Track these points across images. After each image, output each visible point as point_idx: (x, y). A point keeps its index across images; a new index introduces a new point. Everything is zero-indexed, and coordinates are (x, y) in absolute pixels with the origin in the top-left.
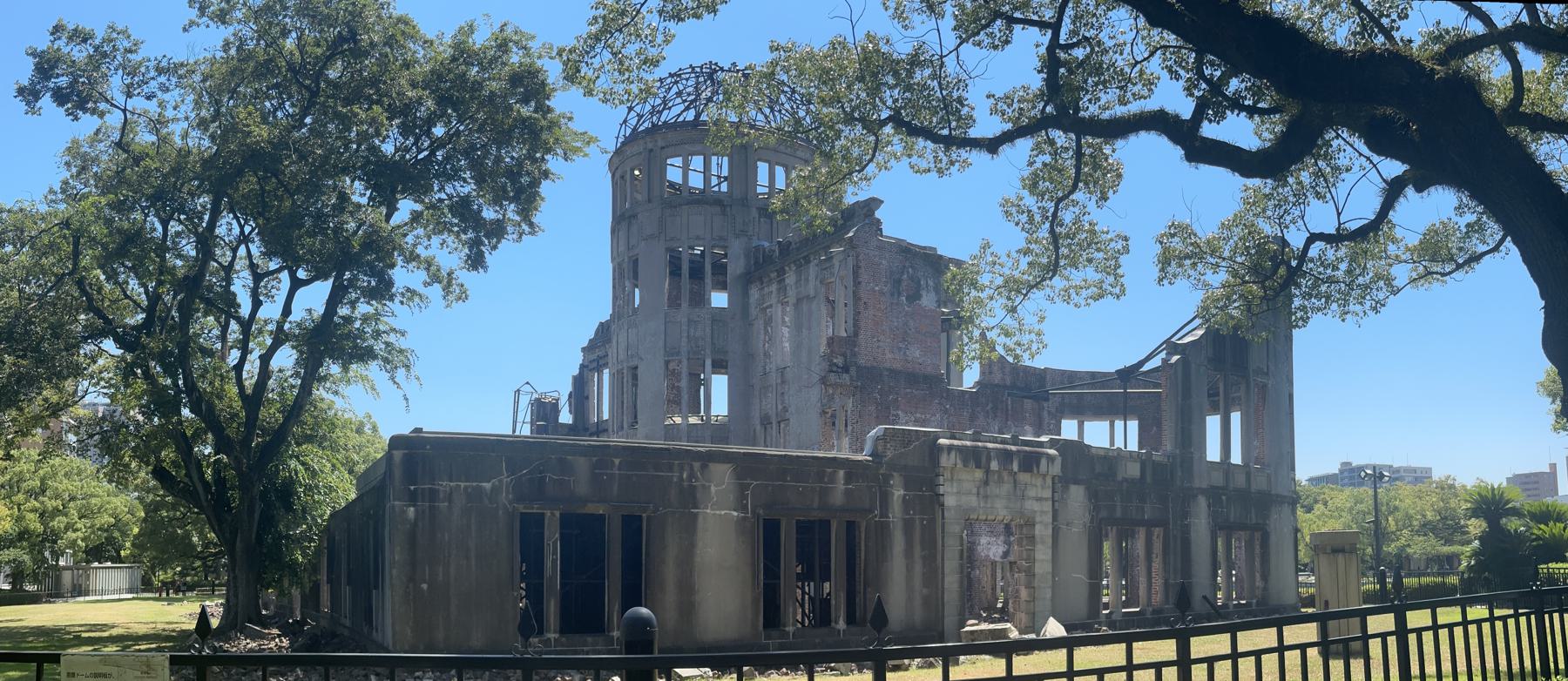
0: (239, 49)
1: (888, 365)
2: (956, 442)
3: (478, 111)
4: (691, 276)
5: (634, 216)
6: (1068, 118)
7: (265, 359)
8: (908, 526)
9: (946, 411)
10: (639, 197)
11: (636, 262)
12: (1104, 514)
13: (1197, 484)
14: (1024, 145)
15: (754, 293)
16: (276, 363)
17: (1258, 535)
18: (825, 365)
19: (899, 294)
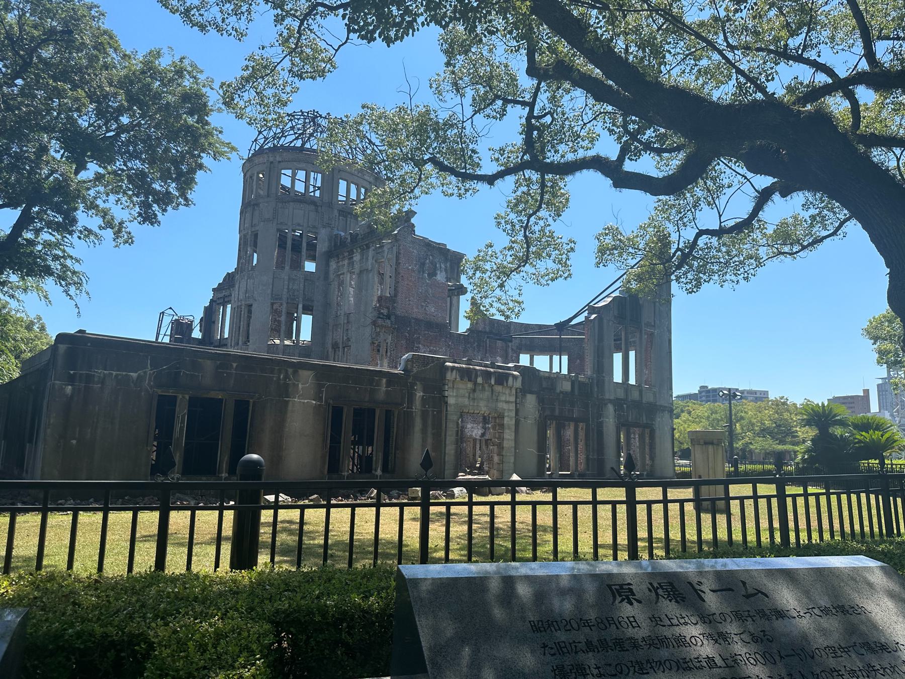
1: (414, 316)
2: (456, 365)
4: (292, 249)
5: (257, 205)
10: (261, 192)
11: (256, 236)
12: (548, 413)
13: (607, 396)
14: (510, 179)
15: (333, 265)
17: (647, 431)
18: (376, 314)
19: (424, 272)
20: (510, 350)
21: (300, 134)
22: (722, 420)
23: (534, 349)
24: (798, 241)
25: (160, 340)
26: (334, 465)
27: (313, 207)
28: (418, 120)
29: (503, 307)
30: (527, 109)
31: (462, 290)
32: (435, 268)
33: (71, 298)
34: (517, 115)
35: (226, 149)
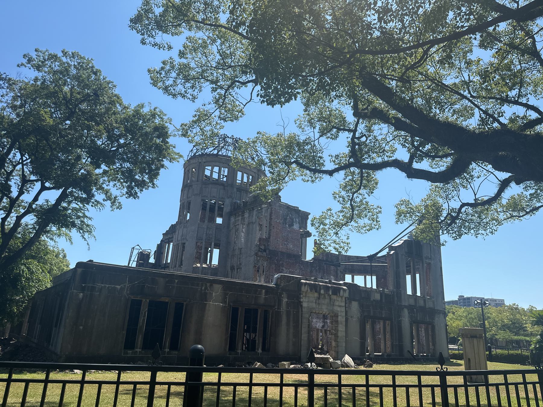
0: (43, 83)
1: (280, 250)
2: (308, 282)
3: (139, 137)
5: (191, 186)
6: (357, 163)
7: (19, 218)
9: (301, 269)
10: (193, 179)
13: (403, 304)
14: (342, 173)
15: (233, 219)
16: (23, 221)
17: (430, 326)
19: (286, 224)
20: (339, 272)
21: (216, 147)
22: (475, 318)
23: (354, 271)
24: (523, 209)
25: (130, 265)
26: (232, 346)
27: (222, 187)
28: (288, 141)
29: (337, 246)
30: (352, 134)
31: (309, 234)
32: (293, 222)
33: (85, 240)
34: (345, 137)
35: (177, 156)
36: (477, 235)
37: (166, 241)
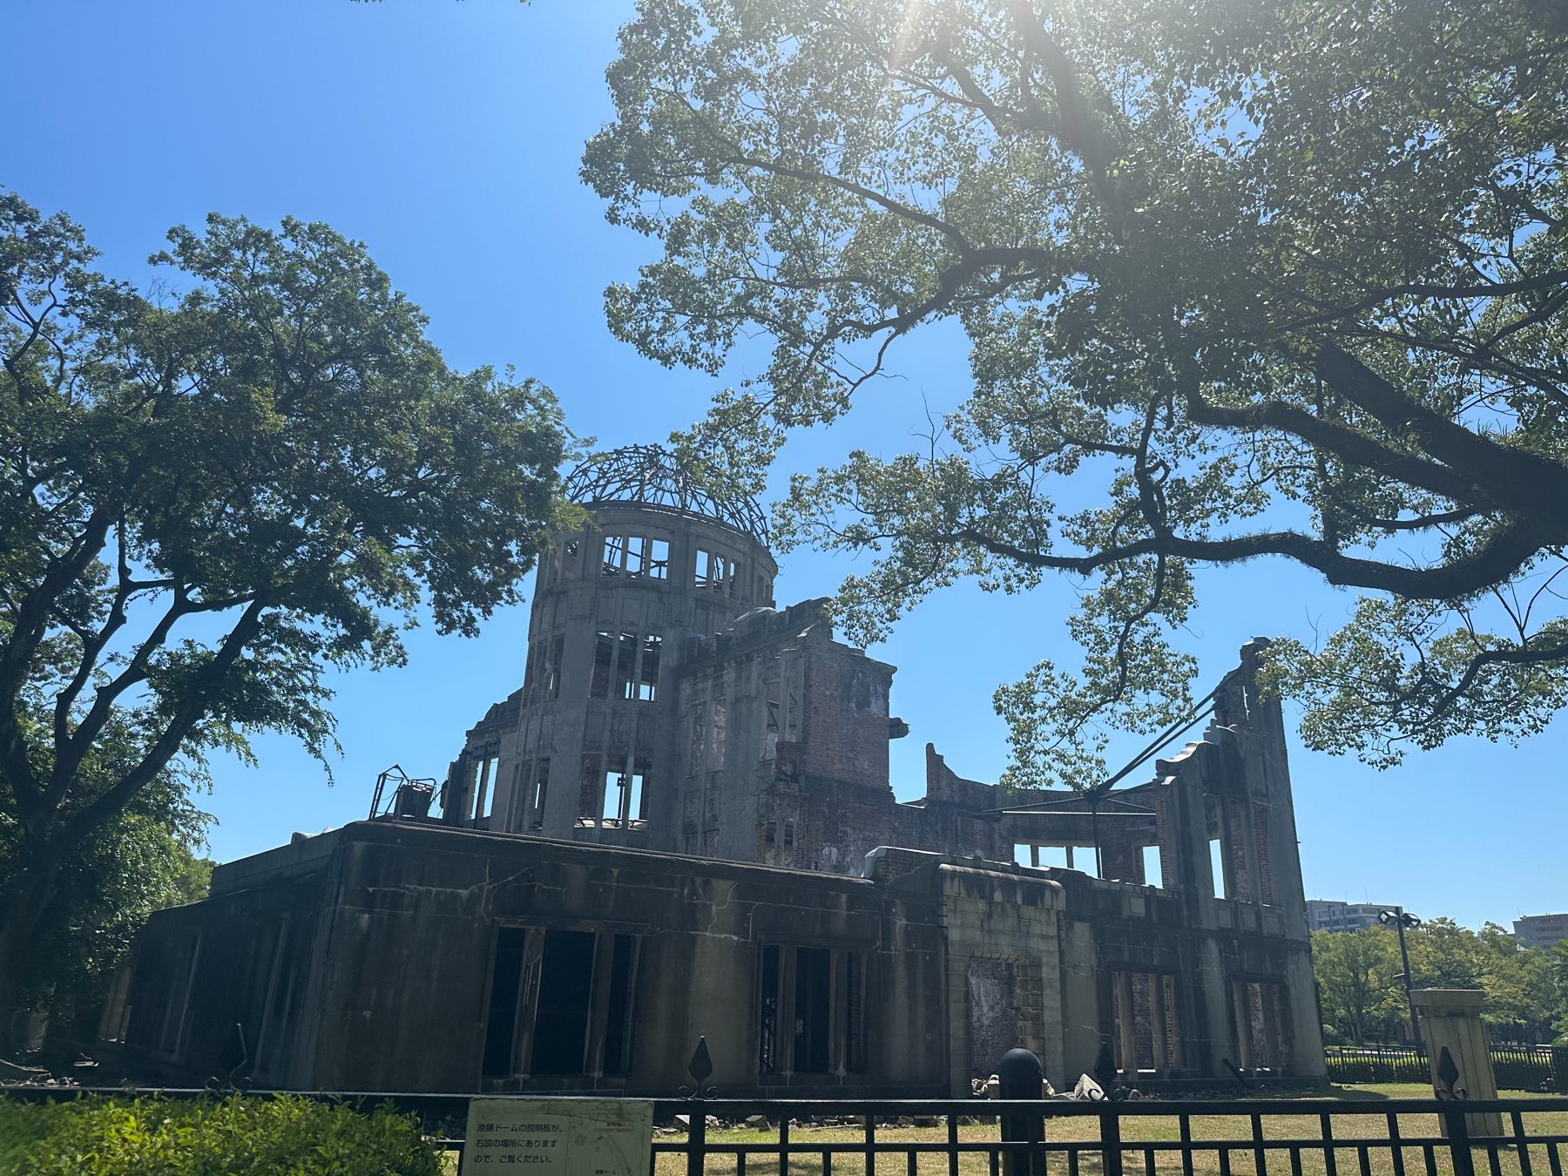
1: (836, 776)
2: (958, 868)
5: (565, 593)
7: (106, 695)
8: (910, 959)
9: (895, 830)
11: (559, 642)
13: (1205, 925)
15: (686, 688)
17: (1276, 987)
23: (1038, 835)
29: (1069, 770)
36: (1493, 734)
37: (479, 752)
